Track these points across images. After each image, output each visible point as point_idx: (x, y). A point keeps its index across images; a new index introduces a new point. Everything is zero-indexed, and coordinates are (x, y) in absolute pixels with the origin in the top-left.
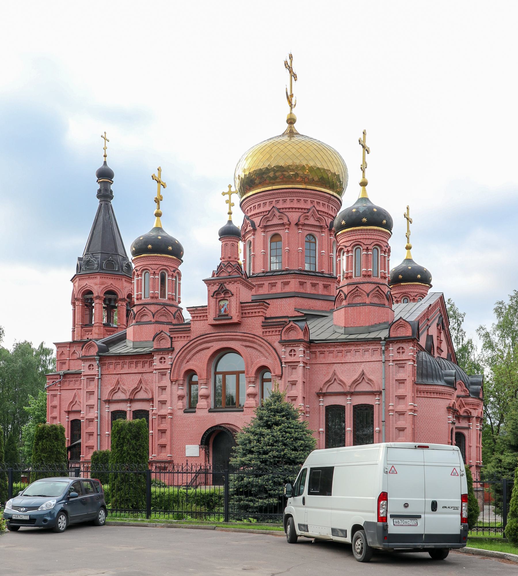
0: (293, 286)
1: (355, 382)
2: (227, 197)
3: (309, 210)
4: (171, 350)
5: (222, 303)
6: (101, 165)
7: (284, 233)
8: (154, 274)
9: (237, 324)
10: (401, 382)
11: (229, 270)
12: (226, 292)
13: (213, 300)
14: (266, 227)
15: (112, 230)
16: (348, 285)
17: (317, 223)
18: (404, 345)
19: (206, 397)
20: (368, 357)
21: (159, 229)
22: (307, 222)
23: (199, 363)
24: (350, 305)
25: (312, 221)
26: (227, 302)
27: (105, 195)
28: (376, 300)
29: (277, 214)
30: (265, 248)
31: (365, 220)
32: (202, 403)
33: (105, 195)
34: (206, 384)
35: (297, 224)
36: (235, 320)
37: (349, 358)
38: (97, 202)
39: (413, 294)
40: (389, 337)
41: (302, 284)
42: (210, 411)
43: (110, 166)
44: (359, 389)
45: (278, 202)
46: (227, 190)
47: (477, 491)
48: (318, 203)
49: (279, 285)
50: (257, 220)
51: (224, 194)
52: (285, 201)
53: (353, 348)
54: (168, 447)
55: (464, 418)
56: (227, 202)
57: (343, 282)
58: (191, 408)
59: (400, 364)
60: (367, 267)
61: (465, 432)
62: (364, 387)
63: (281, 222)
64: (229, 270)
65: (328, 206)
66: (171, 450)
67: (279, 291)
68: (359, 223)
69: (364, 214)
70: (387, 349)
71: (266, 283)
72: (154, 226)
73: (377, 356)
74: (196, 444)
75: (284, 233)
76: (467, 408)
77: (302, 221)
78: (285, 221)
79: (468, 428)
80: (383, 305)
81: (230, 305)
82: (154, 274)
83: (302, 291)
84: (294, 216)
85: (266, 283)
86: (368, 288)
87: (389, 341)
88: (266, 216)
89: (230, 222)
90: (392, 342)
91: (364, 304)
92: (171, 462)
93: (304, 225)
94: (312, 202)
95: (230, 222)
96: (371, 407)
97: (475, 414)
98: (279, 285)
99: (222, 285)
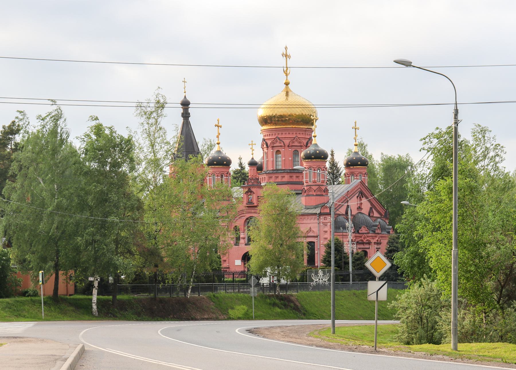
0: (287, 178)
1: (307, 231)
2: (251, 146)
3: (294, 138)
4: (227, 217)
5: (250, 196)
6: (182, 98)
7: (282, 150)
8: (218, 176)
9: (256, 206)
10: (326, 232)
11: (253, 181)
12: (251, 192)
13: (245, 195)
14: (273, 147)
15: (191, 137)
16: (307, 186)
17: (299, 145)
18: (327, 216)
19: (244, 238)
20: (312, 221)
21: (219, 152)
22: (293, 144)
23: (240, 223)
24: (308, 195)
25: (296, 144)
26: (252, 196)
27: (186, 115)
28: (319, 193)
29: (279, 141)
30: (273, 157)
31: (313, 157)
32: (242, 241)
33: (186, 115)
34: (243, 232)
35: (288, 146)
36: (255, 205)
37: (305, 221)
38: (181, 120)
39: (356, 173)
40: (321, 212)
41: (291, 177)
42: (246, 245)
43: (188, 98)
44: (309, 235)
45: (279, 134)
46: (251, 143)
47: (291, 277)
48: (299, 133)
49: (280, 177)
50: (269, 142)
51: (249, 145)
52: (282, 134)
53: (306, 217)
54: (227, 261)
55: (366, 243)
56: (251, 148)
57: (305, 184)
58: (237, 244)
59: (325, 224)
60: (314, 178)
61: (367, 250)
62: (311, 234)
63: (280, 145)
64: (253, 181)
65: (305, 134)
66: (229, 262)
67: (280, 181)
68: (311, 158)
69: (313, 154)
70: (320, 218)
71: (274, 176)
72: (217, 150)
73: (316, 221)
74: (239, 259)
75: (282, 150)
76: (368, 239)
77: (291, 144)
78: (282, 144)
79: (369, 248)
80: (322, 195)
81: (253, 197)
82: (218, 176)
83: (291, 180)
84: (287, 142)
85: (274, 176)
86: (315, 188)
87: (320, 214)
88: (274, 141)
89: (253, 158)
90: (322, 215)
91: (313, 195)
92: (228, 268)
93: (292, 146)
94: (296, 133)
95: (253, 158)
96: (314, 242)
97: (373, 241)
98: (280, 177)
99: (249, 189)
